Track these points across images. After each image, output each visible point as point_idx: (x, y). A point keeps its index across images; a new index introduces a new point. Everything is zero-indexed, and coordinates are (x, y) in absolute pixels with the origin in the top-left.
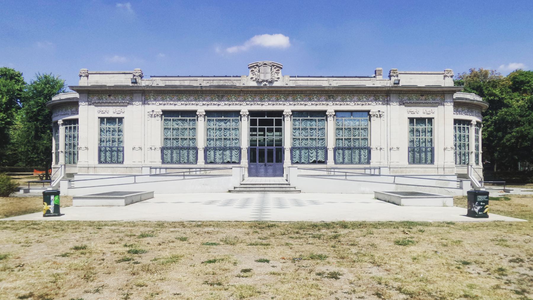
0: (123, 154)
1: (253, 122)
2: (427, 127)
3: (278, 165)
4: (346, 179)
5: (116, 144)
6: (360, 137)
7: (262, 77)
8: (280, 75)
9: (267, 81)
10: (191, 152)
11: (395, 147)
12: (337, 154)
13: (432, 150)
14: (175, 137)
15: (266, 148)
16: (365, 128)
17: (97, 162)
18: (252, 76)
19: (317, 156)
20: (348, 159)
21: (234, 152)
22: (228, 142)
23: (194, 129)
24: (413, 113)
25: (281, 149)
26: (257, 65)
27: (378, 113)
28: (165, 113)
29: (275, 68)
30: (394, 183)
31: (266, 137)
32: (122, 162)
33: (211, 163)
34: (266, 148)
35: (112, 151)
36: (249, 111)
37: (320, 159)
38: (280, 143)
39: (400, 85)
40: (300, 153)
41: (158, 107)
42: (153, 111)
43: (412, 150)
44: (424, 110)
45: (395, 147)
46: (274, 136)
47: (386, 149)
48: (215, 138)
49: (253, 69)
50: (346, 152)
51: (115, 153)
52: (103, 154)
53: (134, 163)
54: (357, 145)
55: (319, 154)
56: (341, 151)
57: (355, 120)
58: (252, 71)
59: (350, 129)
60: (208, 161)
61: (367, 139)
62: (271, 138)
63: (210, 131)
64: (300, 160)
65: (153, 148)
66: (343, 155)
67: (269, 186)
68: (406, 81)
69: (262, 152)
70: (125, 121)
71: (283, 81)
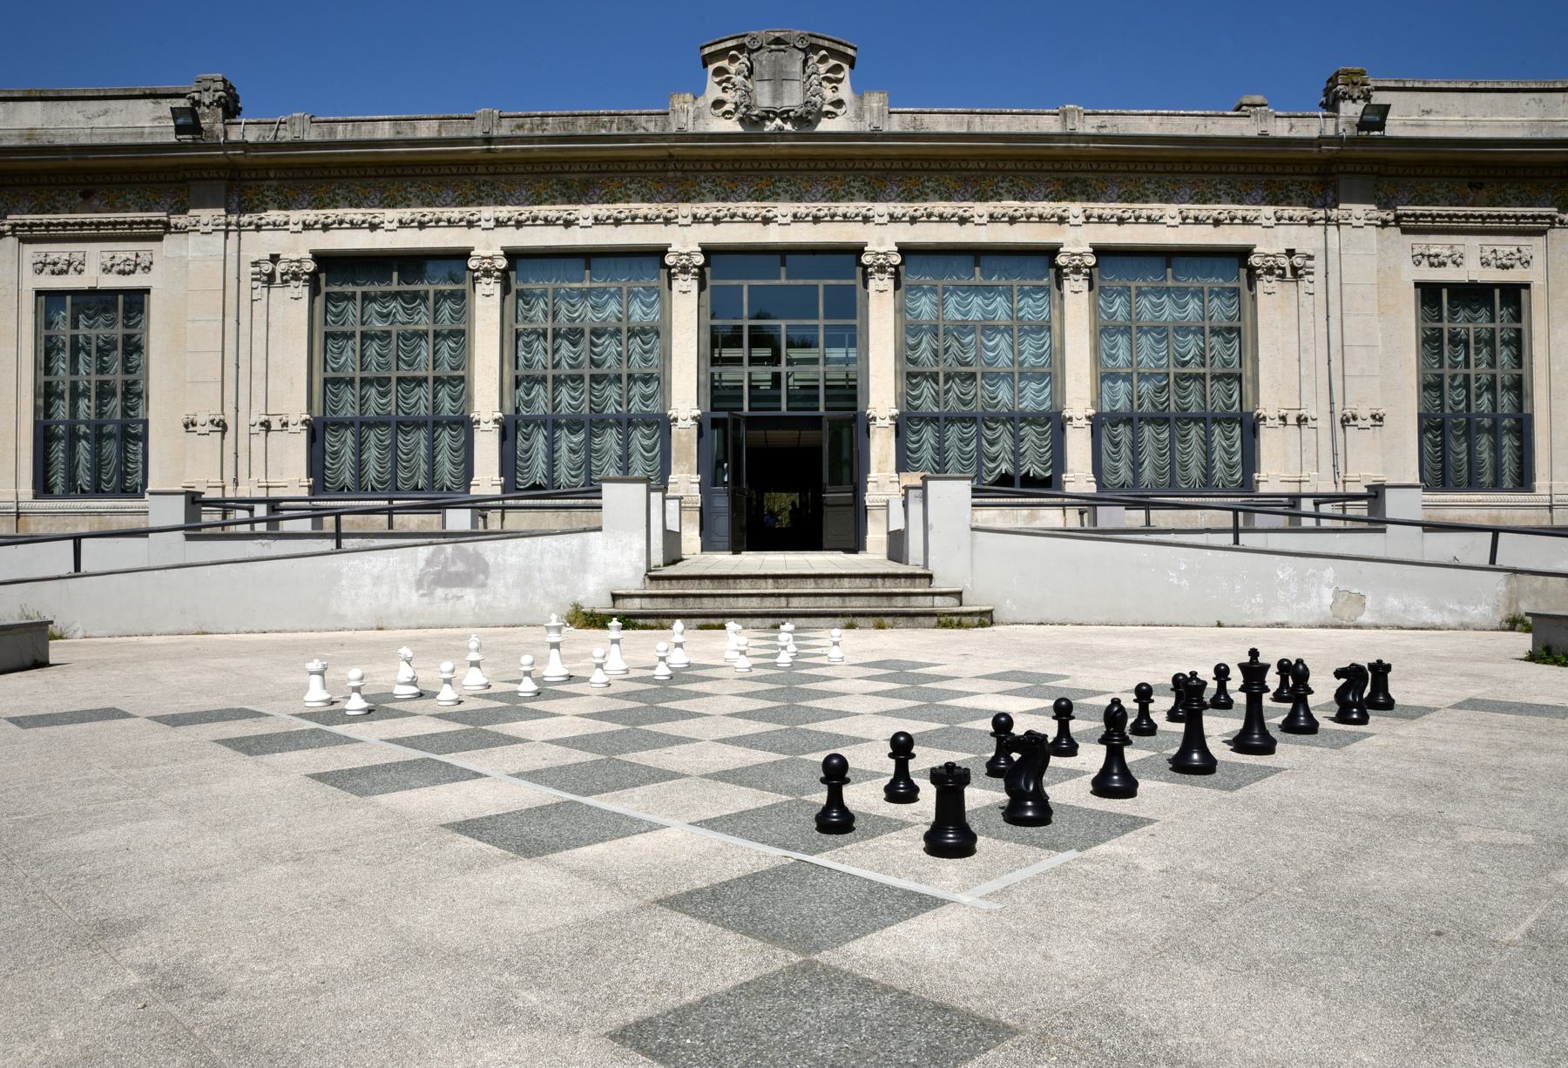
2: (1497, 325)
4: (1236, 547)
6: (1207, 370)
7: (764, 98)
8: (845, 91)
9: (785, 115)
10: (445, 437)
11: (1364, 412)
12: (1105, 443)
13: (1523, 428)
14: (373, 372)
16: (1230, 330)
17: (27, 489)
18: (719, 94)
19: (1017, 455)
20: (1157, 469)
21: (639, 438)
22: (612, 392)
23: (462, 333)
24: (1437, 262)
26: (741, 48)
27: (1285, 262)
28: (329, 263)
29: (823, 60)
30: (1492, 564)
31: (783, 368)
35: (99, 437)
38: (849, 394)
40: (941, 440)
41: (294, 235)
42: (275, 259)
43: (1432, 426)
44: (1488, 249)
45: (1364, 412)
47: (1323, 424)
48: (550, 373)
49: (724, 63)
50: (1148, 431)
51: (110, 448)
52: (59, 451)
54: (1193, 403)
55: (1025, 446)
56: (1123, 432)
57: (1182, 292)
58: (719, 72)
59: (1165, 329)
61: (1239, 378)
62: (804, 373)
63: (528, 345)
65: (275, 425)
66: (1135, 450)
67: (810, 587)
68: (1411, 117)
70: (155, 304)
71: (859, 116)
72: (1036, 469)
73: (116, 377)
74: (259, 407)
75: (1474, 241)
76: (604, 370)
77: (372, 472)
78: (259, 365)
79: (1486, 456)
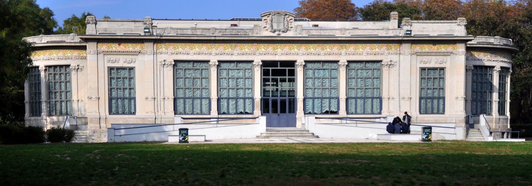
0: (135, 102)
1: (265, 73)
3: (291, 115)
4: (356, 126)
5: (127, 92)
15: (279, 99)
18: (265, 26)
25: (294, 99)
32: (134, 113)
33: (224, 113)
34: (279, 99)
36: (262, 61)
37: (334, 109)
38: (292, 93)
39: (412, 35)
41: (169, 53)
46: (286, 86)
47: (397, 100)
53: (147, 114)
60: (222, 112)
64: (313, 110)
69: (275, 103)
70: (137, 71)
72: (335, 110)
73: (127, 85)
74: (162, 94)
75: (434, 57)
76: (239, 87)
77: (187, 109)
78: (162, 85)
79: (127, 106)
